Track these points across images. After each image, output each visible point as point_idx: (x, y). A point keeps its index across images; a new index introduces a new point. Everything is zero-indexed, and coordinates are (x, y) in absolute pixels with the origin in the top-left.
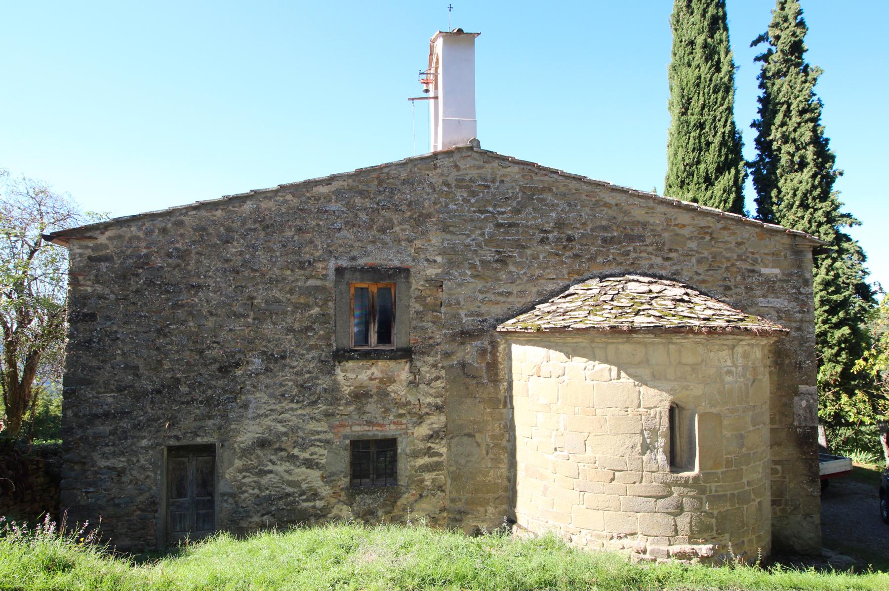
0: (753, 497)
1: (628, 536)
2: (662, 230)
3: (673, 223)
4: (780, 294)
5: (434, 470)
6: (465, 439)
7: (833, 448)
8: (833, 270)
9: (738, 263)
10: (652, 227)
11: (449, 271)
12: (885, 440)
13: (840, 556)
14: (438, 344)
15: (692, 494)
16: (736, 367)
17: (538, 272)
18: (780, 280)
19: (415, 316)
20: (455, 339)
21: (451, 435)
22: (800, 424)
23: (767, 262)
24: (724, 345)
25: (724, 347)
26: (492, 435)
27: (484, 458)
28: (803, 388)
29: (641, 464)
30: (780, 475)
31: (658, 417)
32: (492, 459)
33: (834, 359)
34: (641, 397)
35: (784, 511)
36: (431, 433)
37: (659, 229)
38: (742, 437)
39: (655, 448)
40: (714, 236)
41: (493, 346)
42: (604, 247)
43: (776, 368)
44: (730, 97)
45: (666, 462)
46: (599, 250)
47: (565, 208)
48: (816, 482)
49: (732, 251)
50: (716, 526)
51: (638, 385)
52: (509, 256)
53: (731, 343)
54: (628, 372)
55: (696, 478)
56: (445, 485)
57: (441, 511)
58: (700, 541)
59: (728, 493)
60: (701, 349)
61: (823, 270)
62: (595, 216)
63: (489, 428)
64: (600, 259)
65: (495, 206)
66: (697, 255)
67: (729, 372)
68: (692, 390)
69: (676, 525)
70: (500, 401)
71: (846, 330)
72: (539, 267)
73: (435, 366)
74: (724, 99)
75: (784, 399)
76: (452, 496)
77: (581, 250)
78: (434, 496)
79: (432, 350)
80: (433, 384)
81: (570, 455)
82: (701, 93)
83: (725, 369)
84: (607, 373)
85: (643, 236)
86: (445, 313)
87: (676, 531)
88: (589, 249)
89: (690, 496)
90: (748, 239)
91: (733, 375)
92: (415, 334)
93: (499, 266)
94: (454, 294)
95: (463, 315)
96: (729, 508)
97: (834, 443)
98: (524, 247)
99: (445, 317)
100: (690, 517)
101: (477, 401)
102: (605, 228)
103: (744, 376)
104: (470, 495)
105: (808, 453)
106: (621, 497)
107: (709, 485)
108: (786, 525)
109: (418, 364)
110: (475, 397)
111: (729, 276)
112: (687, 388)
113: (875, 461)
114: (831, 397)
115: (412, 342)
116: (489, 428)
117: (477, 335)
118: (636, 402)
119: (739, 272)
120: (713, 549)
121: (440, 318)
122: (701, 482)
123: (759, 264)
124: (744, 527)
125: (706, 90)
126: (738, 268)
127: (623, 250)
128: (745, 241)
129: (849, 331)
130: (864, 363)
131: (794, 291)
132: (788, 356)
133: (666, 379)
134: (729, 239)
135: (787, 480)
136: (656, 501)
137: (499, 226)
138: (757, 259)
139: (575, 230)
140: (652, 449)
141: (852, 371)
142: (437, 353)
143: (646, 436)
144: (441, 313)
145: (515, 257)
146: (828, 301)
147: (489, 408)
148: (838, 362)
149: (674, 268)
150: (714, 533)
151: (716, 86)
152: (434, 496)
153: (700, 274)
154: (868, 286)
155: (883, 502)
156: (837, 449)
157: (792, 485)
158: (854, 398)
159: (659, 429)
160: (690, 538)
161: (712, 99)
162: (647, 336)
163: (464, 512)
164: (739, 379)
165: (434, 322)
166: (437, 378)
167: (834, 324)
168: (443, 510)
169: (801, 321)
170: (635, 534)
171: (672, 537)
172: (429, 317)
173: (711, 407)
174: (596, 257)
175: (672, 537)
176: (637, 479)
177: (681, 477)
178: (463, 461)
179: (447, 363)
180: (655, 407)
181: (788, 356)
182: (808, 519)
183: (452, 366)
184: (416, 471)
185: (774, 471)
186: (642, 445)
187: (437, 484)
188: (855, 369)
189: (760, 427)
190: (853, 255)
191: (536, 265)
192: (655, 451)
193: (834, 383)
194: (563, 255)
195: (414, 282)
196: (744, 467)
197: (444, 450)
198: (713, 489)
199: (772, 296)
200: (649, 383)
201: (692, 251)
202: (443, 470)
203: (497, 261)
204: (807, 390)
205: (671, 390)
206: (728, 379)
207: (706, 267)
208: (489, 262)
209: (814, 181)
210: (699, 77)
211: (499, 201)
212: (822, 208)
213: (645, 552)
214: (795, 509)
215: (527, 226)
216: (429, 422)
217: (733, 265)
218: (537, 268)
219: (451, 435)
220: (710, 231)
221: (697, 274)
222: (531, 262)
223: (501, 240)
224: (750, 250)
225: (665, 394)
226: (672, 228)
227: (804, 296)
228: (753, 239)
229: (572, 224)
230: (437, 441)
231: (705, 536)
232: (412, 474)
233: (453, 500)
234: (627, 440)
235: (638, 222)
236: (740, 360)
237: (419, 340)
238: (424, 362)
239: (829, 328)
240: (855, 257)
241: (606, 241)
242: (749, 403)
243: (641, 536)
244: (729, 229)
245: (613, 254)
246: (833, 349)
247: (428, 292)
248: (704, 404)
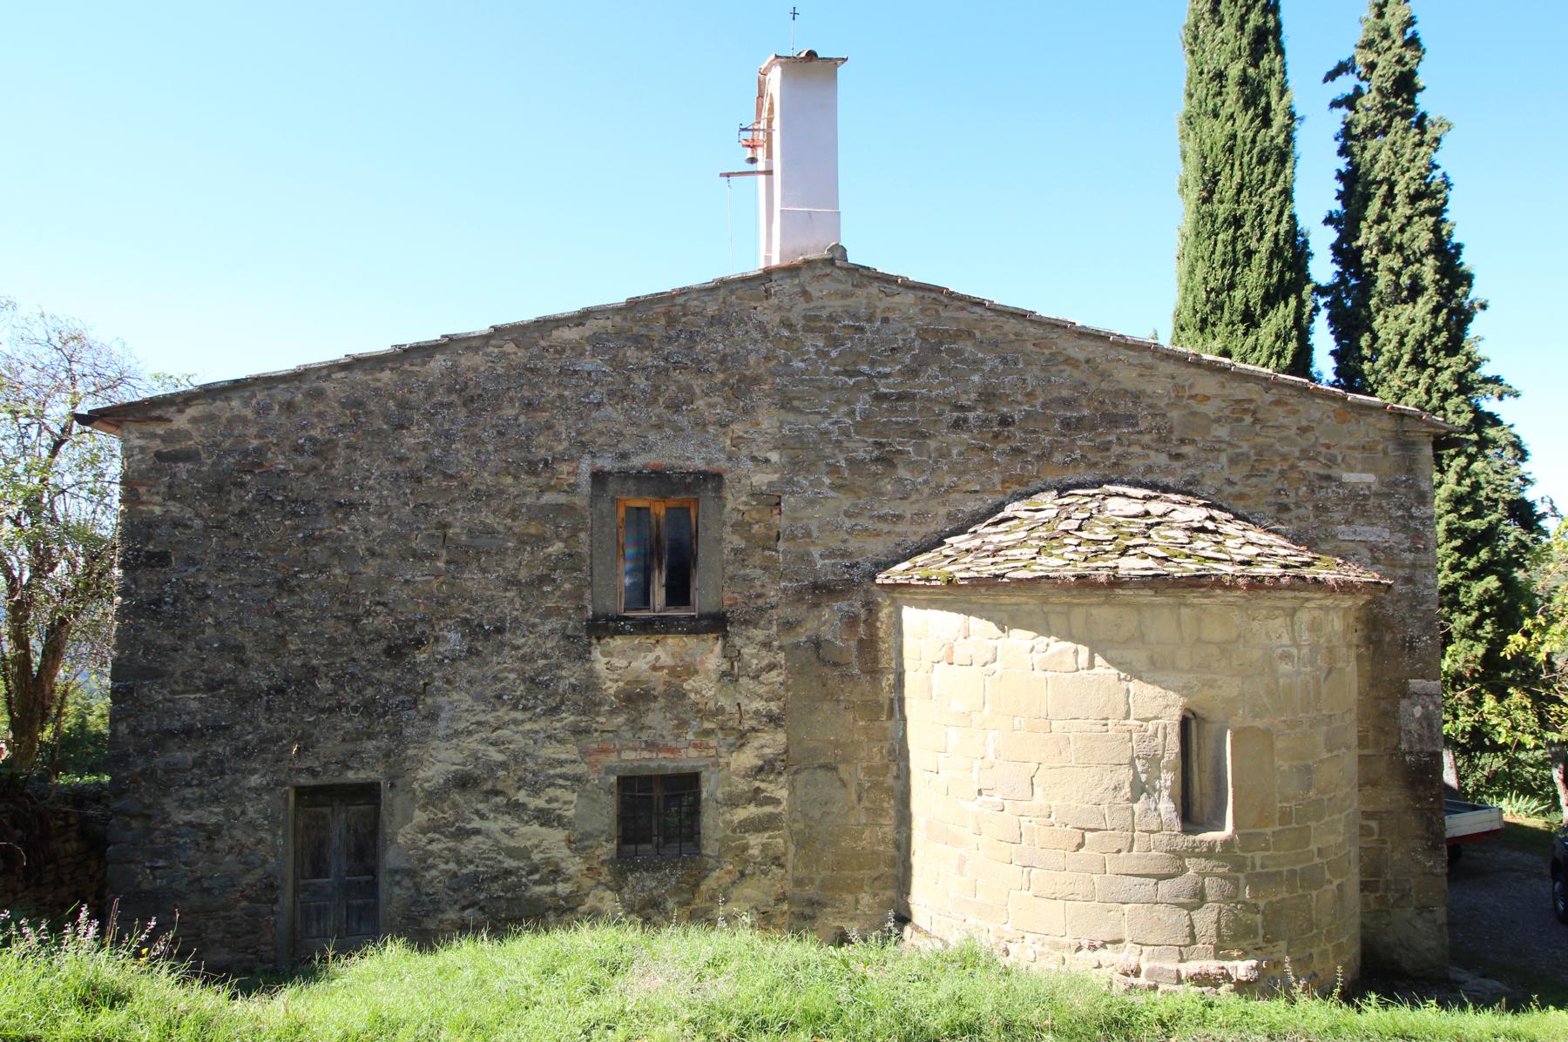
0: (1327, 876)
1: (1108, 946)
2: (1168, 405)
3: (1187, 394)
4: (1376, 518)
5: (766, 829)
6: (820, 774)
7: (1470, 790)
8: (1469, 475)
9: (1301, 464)
10: (1149, 401)
11: (791, 478)
14: (772, 607)
15: (1221, 870)
16: (1299, 647)
17: (948, 480)
18: (1376, 494)
19: (732, 557)
20: (803, 598)
21: (795, 768)
22: (1411, 747)
23: (1353, 462)
24: (1277, 608)
25: (1277, 613)
26: (868, 767)
27: (853, 808)
28: (1416, 684)
29: (1130, 818)
30: (1375, 837)
31: (1160, 734)
32: (868, 810)
33: (1471, 633)
34: (1131, 700)
35: (1382, 900)
36: (760, 763)
37: (1162, 404)
38: (1308, 770)
39: (1155, 790)
40: (1259, 416)
41: (870, 611)
42: (1065, 436)
43: (1368, 648)
44: (1288, 171)
45: (1174, 814)
46: (1057, 442)
47: (997, 367)
48: (1440, 849)
49: (1292, 443)
50: (1263, 927)
51: (1125, 679)
52: (898, 451)
53: (1288, 604)
54: (1108, 656)
55: (1227, 844)
56: (785, 854)
57: (779, 901)
58: (1235, 953)
59: (1285, 869)
60: (1236, 616)
61: (1451, 477)
62: (1049, 381)
63: (863, 754)
64: (1058, 457)
65: (873, 363)
66: (1230, 450)
67: (1286, 657)
68: (1220, 687)
69: (1192, 926)
70: (881, 706)
71: (1492, 582)
72: (951, 471)
73: (766, 645)
74: (1276, 174)
75: (1383, 704)
76: (796, 874)
77: (1025, 440)
78: (766, 875)
79: (761, 617)
80: (764, 677)
81: (1006, 802)
82: (1237, 163)
83: (1279, 651)
84: (1070, 659)
85: (1134, 417)
86: (785, 553)
87: (1193, 936)
88: (1038, 438)
89: (1217, 875)
90: (1320, 422)
91: (1293, 661)
93: (880, 468)
94: (802, 519)
95: (816, 556)
96: (1287, 895)
97: (1470, 782)
98: (923, 436)
99: (785, 559)
100: (1217, 911)
101: (842, 706)
102: (1067, 403)
103: (1312, 662)
104: (829, 873)
105: (1426, 799)
106: (1095, 876)
107: (1250, 855)
108: (1387, 925)
109: (738, 641)
110: (838, 701)
111: (1286, 486)
112: (1211, 684)
113: (1543, 813)
114: (1466, 699)
115: (727, 602)
116: (863, 754)
117: (842, 591)
118: (1122, 709)
119: (1303, 480)
120: (1257, 968)
121: (776, 561)
122: (1237, 850)
123: (1339, 465)
124: (1311, 930)
125: (1246, 159)
126: (1301, 472)
127: (1098, 441)
128: (1313, 425)
129: (1497, 584)
130: (1524, 640)
131: (1400, 513)
132: (1389, 627)
133: (1174, 668)
134: (1286, 421)
135: (1389, 846)
136: (1156, 884)
137: (880, 398)
138: (1335, 456)
139: (1014, 405)
140: (1151, 791)
141: (1502, 654)
142: (770, 622)
143: (1140, 769)
144: (777, 552)
145: (909, 452)
146: (1461, 531)
147: (862, 719)
148: (1478, 639)
149: (1190, 472)
150: (1260, 939)
151: (1262, 151)
152: (766, 875)
153: (1235, 484)
154: (1531, 505)
155: (1558, 884)
156: (1477, 792)
157: (1397, 856)
158: (1506, 702)
159: (1163, 757)
160: (1217, 949)
161: (1255, 175)
162: (1141, 592)
163: (819, 903)
164: (1303, 669)
165: (765, 569)
166: (771, 667)
167: (1471, 571)
168: (781, 899)
169: (1413, 566)
170: (1120, 941)
171: (1185, 946)
172: (757, 559)
173: (1254, 717)
174: (1051, 454)
175: (1185, 946)
176: (1124, 844)
177: (1201, 841)
178: (816, 813)
179: (788, 640)
180: (1156, 718)
181: (1389, 627)
182: (1425, 914)
183: (797, 646)
184: (734, 831)
185: (1365, 831)
186: (1132, 785)
187: (770, 853)
188: (1508, 651)
189: (1341, 753)
190: (1504, 449)
191: (946, 468)
192: (1156, 795)
193: (1472, 675)
194: (992, 449)
195: (730, 497)
196: (1312, 824)
197: (783, 794)
198: (1258, 862)
199: (1362, 521)
200: (1144, 675)
201: (1221, 442)
202: (782, 828)
203: (877, 460)
204: (1423, 688)
205: (1184, 687)
206: (1285, 667)
207: (1245, 470)
208: (863, 461)
209: (1436, 318)
210: (1234, 137)
211: (880, 354)
212: (1449, 366)
213: (1137, 973)
214: (1402, 897)
215: (929, 399)
216: (756, 744)
217: (1293, 467)
218: (948, 473)
219: (795, 768)
220: (1252, 407)
221: (1230, 483)
222: (936, 462)
223: (884, 424)
224: (1322, 441)
225: (1172, 695)
226: (1185, 402)
227: (1418, 522)
228: (1328, 421)
229: (1008, 396)
230: (772, 777)
231: (1244, 944)
232: (727, 836)
233: (799, 882)
234: (1106, 776)
235: (1126, 392)
236: (1306, 635)
237: (740, 599)
238: (748, 638)
239: (1462, 578)
240: (1509, 453)
241: (1068, 424)
242: (1320, 710)
243: (1130, 945)
244: (1286, 404)
245: (1081, 448)
246: (1469, 615)
247: (754, 514)
248: (1241, 712)
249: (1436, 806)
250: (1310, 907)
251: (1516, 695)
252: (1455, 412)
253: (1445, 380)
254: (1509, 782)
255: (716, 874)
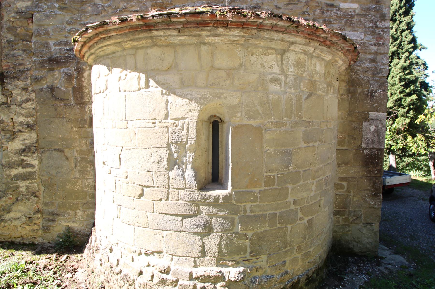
0: (300, 215)
4: (357, 27)
5: (28, 179)
6: (55, 154)
7: (400, 168)
8: (409, 59)
11: (38, 4)
12: (433, 164)
13: (394, 256)
14: (28, 70)
15: (222, 213)
16: (286, 76)
18: (358, 15)
19: (7, 44)
20: (44, 66)
21: (42, 150)
22: (367, 146)
25: (270, 51)
26: (79, 151)
27: (72, 170)
28: (373, 114)
29: (167, 180)
30: (345, 190)
31: (185, 129)
32: (80, 171)
33: (405, 115)
34: (169, 107)
35: (346, 219)
36: (24, 147)
38: (289, 153)
39: (183, 164)
41: (79, 72)
43: (348, 96)
45: (193, 179)
48: (378, 196)
53: (279, 46)
54: (157, 80)
55: (226, 197)
56: (38, 191)
57: (36, 212)
58: (230, 263)
59: (268, 213)
60: (239, 52)
61: (403, 60)
63: (76, 144)
67: (275, 80)
68: (225, 98)
69: (203, 246)
70: (85, 121)
71: (414, 97)
73: (25, 89)
75: (354, 124)
76: (45, 200)
78: (29, 200)
79: (22, 74)
80: (24, 105)
83: (270, 76)
86: (35, 43)
87: (203, 253)
89: (221, 217)
91: (280, 84)
92: (7, 60)
94: (44, 25)
95: (52, 44)
96: (268, 228)
97: (401, 166)
99: (35, 46)
100: (219, 238)
101: (65, 120)
103: (296, 86)
104: (62, 200)
105: (373, 171)
106: (148, 214)
107: (243, 204)
108: (347, 231)
109: (10, 87)
110: (63, 118)
111: (308, 10)
112: (219, 96)
113: (425, 176)
114: (401, 138)
115: (4, 68)
116: (76, 144)
117: (64, 62)
119: (318, 6)
120: (244, 272)
121: (31, 47)
122: (233, 201)
124: (286, 247)
129: (416, 97)
130: (424, 117)
131: (371, 25)
132: (360, 85)
133: (196, 86)
135: (352, 194)
136: (182, 220)
140: (180, 164)
141: (416, 122)
142: (27, 78)
143: (173, 150)
144: (31, 42)
146: (404, 79)
148: (407, 117)
150: (248, 256)
152: (29, 200)
154: (427, 84)
155: (432, 206)
156: (402, 169)
157: (356, 199)
158: (415, 139)
159: (187, 143)
160: (218, 260)
162: (169, 32)
163: (57, 214)
164: (288, 90)
165: (24, 51)
166: (28, 100)
167: (407, 93)
168: (37, 212)
169: (376, 53)
170: (161, 252)
171: (198, 258)
172: (20, 45)
173: (249, 118)
175: (198, 258)
176: (164, 196)
178: (53, 172)
179: (37, 87)
180: (183, 118)
181: (360, 85)
182: (368, 227)
183: (41, 90)
184: (12, 179)
185: (338, 186)
186: (168, 160)
187: (30, 190)
188: (418, 121)
189: (316, 144)
190: (420, 66)
192: (184, 166)
193: (404, 129)
195: (5, 14)
196: (290, 186)
197: (36, 162)
198: (248, 209)
199: (350, 29)
200: (177, 91)
202: (36, 179)
204: (377, 116)
205: (201, 98)
206: (273, 87)
209: (401, 3)
212: (405, 20)
214: (356, 219)
216: (21, 138)
219: (42, 150)
225: (194, 106)
227: (380, 30)
230: (29, 154)
231: (237, 258)
232: (8, 182)
233: (47, 204)
236: (292, 69)
237: (11, 66)
238: (15, 86)
239: (404, 96)
240: (422, 67)
242: (301, 117)
246: (405, 109)
247: (19, 23)
248: (239, 114)
249: (378, 175)
250: (285, 235)
251: (419, 136)
252: (405, 37)
253: (403, 26)
254: (412, 166)
255: (4, 199)
